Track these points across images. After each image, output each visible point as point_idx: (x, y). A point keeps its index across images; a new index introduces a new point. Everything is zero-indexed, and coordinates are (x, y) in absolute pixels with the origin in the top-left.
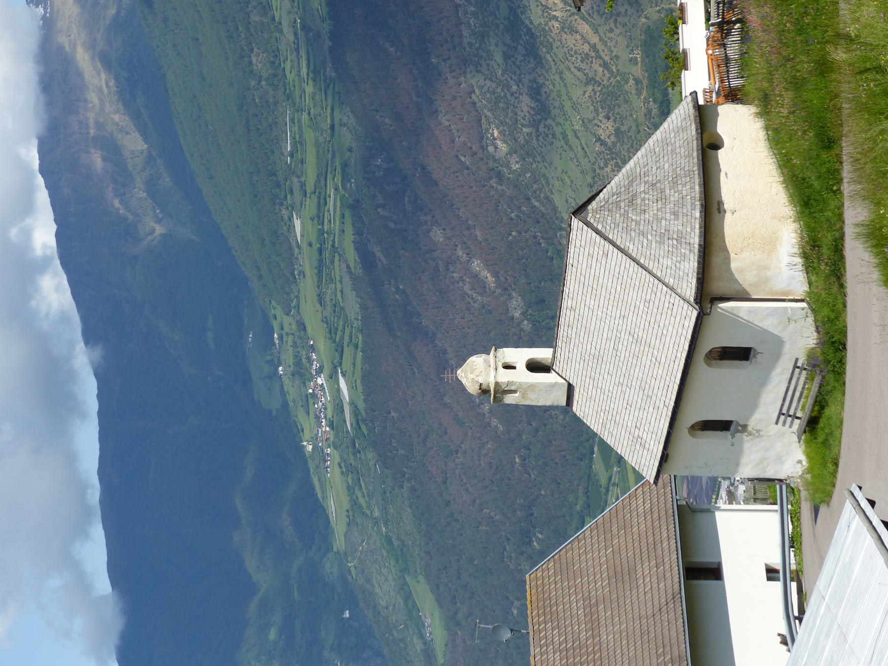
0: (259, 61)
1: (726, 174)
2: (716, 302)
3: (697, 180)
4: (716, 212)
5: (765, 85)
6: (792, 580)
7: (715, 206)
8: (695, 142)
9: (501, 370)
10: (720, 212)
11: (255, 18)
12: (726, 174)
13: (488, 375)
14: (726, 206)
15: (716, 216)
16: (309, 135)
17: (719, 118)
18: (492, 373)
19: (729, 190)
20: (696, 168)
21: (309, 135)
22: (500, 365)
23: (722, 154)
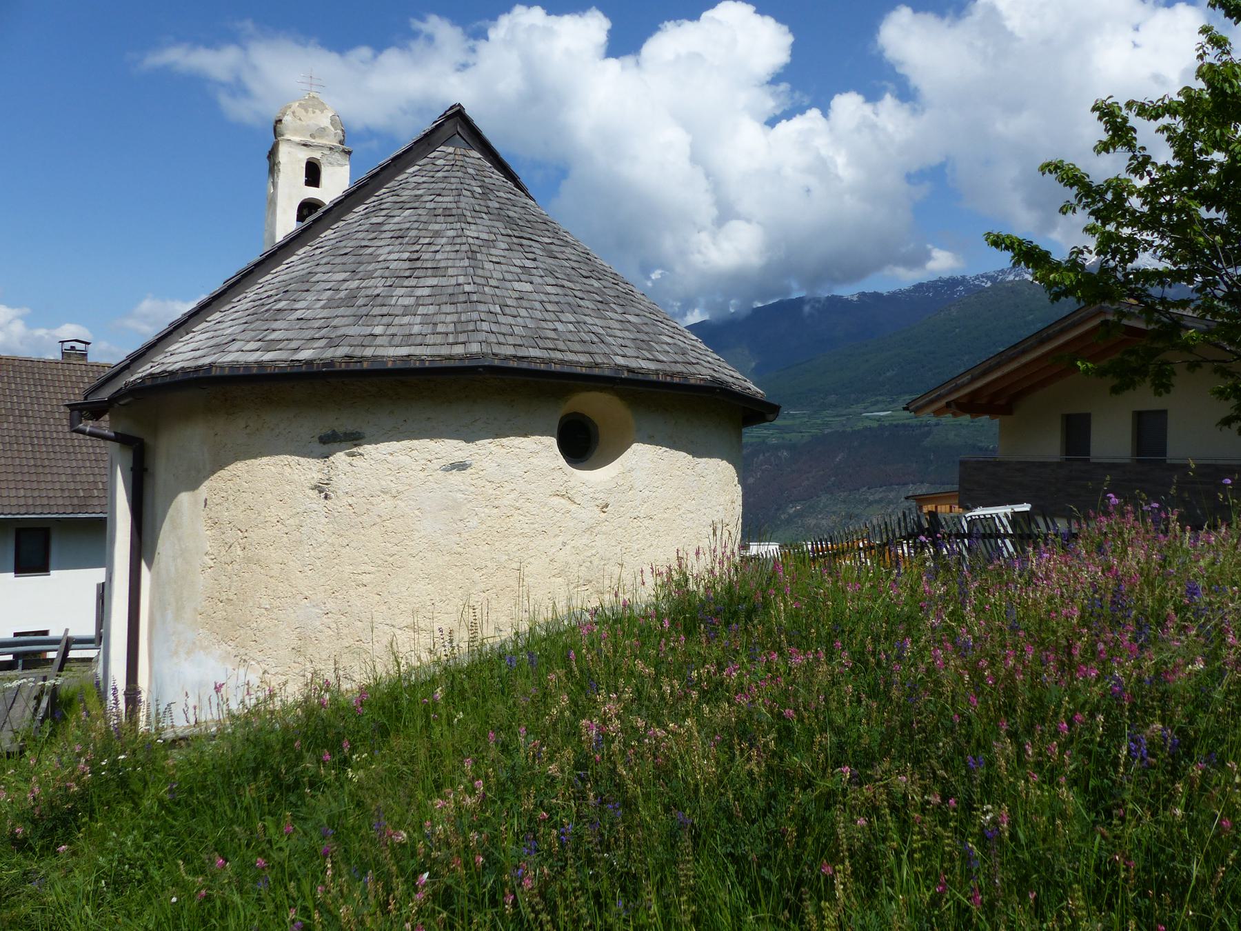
0: (833, 398)
1: (461, 466)
2: (128, 457)
3: (430, 349)
4: (326, 431)
5: (780, 610)
6: (16, 655)
7: (344, 422)
8: (583, 359)
9: (304, 155)
10: (324, 440)
11: (853, 396)
12: (461, 466)
13: (296, 131)
14: (340, 458)
15: (311, 425)
16: (797, 421)
17: (682, 458)
18: (297, 139)
19: (401, 472)
20: (475, 348)
21: (797, 421)
22: (317, 155)
23: (540, 452)
